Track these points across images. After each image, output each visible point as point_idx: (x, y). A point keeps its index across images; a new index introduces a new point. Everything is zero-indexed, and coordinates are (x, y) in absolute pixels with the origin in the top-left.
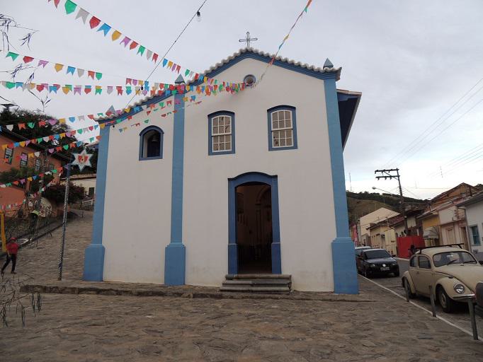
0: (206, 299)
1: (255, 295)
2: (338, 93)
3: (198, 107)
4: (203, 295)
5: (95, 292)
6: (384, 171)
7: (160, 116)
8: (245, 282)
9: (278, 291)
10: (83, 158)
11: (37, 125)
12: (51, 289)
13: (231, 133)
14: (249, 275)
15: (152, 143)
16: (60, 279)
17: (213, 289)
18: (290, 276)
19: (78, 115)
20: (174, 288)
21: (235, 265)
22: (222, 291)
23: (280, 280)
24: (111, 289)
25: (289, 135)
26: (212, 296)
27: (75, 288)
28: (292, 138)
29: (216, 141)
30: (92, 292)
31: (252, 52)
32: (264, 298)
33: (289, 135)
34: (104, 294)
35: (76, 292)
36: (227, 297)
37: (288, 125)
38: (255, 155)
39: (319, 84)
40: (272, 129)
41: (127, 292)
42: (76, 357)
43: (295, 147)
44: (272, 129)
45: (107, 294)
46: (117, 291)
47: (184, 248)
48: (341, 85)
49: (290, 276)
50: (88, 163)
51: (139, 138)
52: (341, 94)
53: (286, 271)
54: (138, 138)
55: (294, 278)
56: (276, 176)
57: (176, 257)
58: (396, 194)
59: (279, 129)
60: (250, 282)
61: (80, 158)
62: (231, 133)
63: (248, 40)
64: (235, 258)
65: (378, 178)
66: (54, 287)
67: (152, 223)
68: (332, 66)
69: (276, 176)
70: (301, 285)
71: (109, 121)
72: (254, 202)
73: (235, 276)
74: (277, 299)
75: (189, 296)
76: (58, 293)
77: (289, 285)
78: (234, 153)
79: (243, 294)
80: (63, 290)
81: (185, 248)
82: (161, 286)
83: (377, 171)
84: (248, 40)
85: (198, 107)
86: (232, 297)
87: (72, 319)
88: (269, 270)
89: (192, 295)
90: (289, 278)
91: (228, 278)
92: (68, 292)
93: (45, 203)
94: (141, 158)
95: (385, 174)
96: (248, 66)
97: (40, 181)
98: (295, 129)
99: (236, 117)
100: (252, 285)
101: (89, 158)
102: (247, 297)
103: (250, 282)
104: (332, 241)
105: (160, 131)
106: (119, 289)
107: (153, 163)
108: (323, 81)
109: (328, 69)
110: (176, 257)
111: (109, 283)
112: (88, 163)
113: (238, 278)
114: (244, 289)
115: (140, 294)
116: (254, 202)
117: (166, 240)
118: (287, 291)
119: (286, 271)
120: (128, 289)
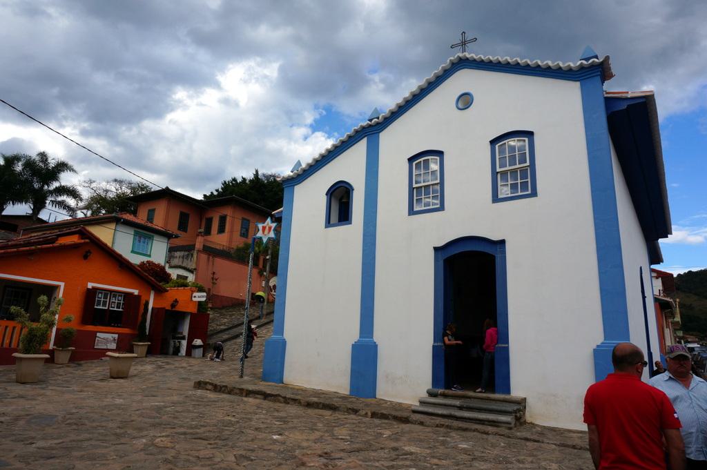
0: (386, 421)
2: (606, 99)
4: (398, 416)
5: (262, 397)
7: (350, 167)
9: (494, 422)
10: (267, 228)
11: (274, 179)
12: (221, 387)
13: (438, 181)
16: (241, 377)
20: (360, 401)
21: (442, 375)
22: (414, 412)
23: (504, 404)
24: (279, 395)
25: (524, 176)
26: (396, 418)
28: (529, 180)
29: (419, 193)
30: (259, 396)
32: (466, 430)
33: (524, 176)
34: (270, 401)
35: (244, 394)
37: (523, 160)
38: (470, 211)
39: (571, 93)
40: (498, 170)
41: (295, 400)
42: (500, 466)
43: (534, 194)
44: (498, 170)
45: (275, 401)
46: (285, 398)
47: (375, 346)
48: (612, 87)
49: (525, 399)
50: (272, 235)
53: (517, 392)
54: (323, 200)
55: (530, 402)
56: (503, 242)
57: (365, 357)
58: (69, 356)
59: (508, 168)
60: (457, 403)
61: (264, 228)
62: (438, 181)
63: (464, 44)
64: (442, 366)
66: (224, 386)
69: (503, 242)
70: (538, 414)
73: (440, 391)
74: (487, 433)
75: (366, 414)
76: (226, 393)
79: (439, 421)
80: (232, 390)
81: (377, 346)
82: (344, 398)
84: (464, 44)
85: (397, 145)
86: (422, 423)
87: (188, 428)
88: (491, 387)
89: (370, 414)
90: (522, 403)
91: (431, 394)
92: (236, 394)
94: (328, 224)
96: (464, 81)
98: (533, 165)
99: (536, 138)
100: (461, 408)
101: (273, 229)
102: (442, 426)
103: (457, 403)
104: (595, 347)
105: (349, 188)
107: (343, 229)
108: (578, 84)
109: (584, 62)
110: (365, 357)
111: (286, 387)
112: (272, 235)
113: (445, 396)
114: (445, 412)
115: (309, 405)
116: (471, 279)
117: (354, 334)
119: (517, 392)
120: (297, 397)
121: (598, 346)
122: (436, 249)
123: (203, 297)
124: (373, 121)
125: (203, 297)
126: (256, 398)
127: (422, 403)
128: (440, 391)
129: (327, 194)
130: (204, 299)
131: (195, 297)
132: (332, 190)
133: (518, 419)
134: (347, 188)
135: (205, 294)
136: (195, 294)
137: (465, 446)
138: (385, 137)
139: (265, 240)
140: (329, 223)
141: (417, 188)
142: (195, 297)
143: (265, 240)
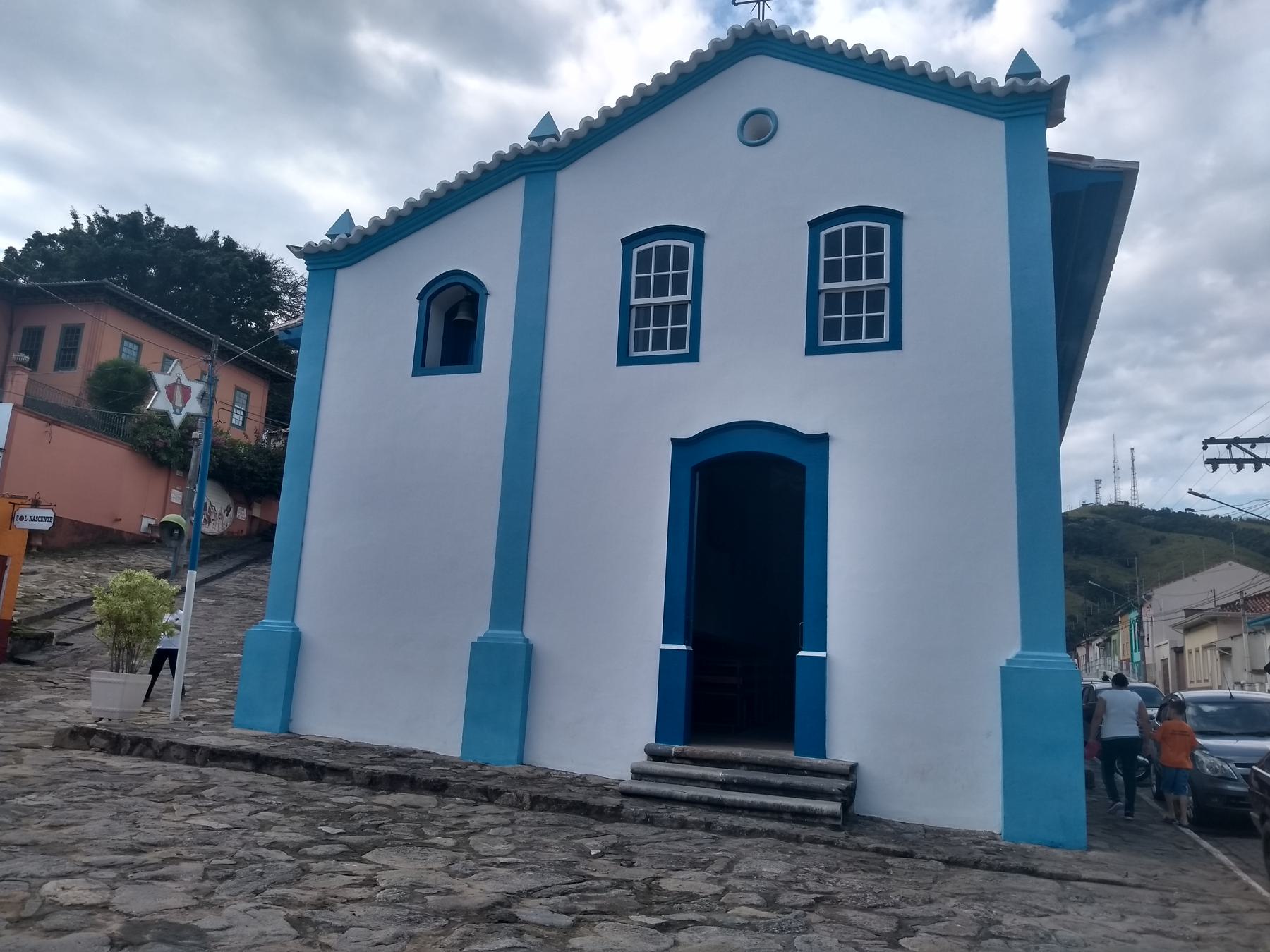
1: (724, 820)
3: (595, 220)
4: (580, 803)
6: (1236, 441)
7: (484, 247)
8: (705, 773)
12: (136, 742)
14: (740, 752)
15: (451, 327)
17: (603, 787)
18: (854, 768)
19: (275, 241)
22: (626, 794)
27: (197, 747)
31: (771, 34)
36: (633, 819)
37: (875, 270)
38: (754, 374)
39: (995, 130)
43: (895, 343)
50: (194, 407)
51: (415, 305)
52: (1067, 171)
56: (822, 440)
60: (719, 773)
65: (1215, 463)
67: (458, 582)
68: (1039, 74)
69: (823, 439)
70: (899, 797)
71: (344, 251)
72: (747, 524)
73: (675, 748)
77: (848, 797)
78: (697, 360)
83: (1212, 441)
85: (595, 220)
86: (649, 821)
89: (526, 799)
92: (177, 759)
93: (216, 499)
94: (421, 366)
95: (1237, 453)
96: (763, 82)
97: (195, 435)
98: (896, 284)
100: (725, 785)
105: (478, 290)
106: (321, 761)
108: (1000, 125)
109: (1020, 82)
111: (305, 742)
112: (194, 407)
115: (374, 783)
116: (747, 524)
118: (833, 816)
121: (1009, 661)
122: (675, 442)
123: (44, 519)
124: (545, 143)
125: (44, 519)
126: (236, 769)
127: (638, 774)
128: (675, 748)
129: (420, 297)
130: (46, 526)
131: (22, 518)
132: (438, 286)
133: (846, 806)
134: (467, 288)
135: (50, 513)
136: (22, 512)
137: (392, 769)
138: (571, 185)
139: (177, 420)
140: (423, 364)
141: (638, 308)
142: (22, 518)
143: (177, 420)
